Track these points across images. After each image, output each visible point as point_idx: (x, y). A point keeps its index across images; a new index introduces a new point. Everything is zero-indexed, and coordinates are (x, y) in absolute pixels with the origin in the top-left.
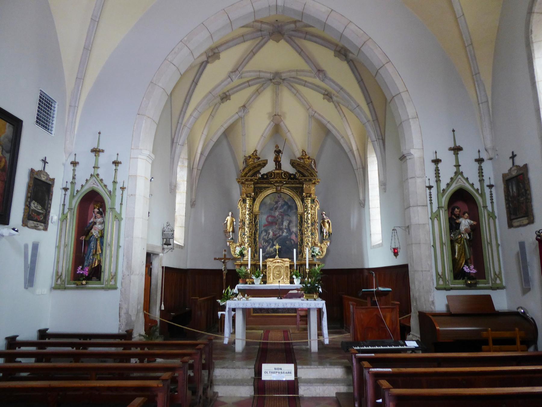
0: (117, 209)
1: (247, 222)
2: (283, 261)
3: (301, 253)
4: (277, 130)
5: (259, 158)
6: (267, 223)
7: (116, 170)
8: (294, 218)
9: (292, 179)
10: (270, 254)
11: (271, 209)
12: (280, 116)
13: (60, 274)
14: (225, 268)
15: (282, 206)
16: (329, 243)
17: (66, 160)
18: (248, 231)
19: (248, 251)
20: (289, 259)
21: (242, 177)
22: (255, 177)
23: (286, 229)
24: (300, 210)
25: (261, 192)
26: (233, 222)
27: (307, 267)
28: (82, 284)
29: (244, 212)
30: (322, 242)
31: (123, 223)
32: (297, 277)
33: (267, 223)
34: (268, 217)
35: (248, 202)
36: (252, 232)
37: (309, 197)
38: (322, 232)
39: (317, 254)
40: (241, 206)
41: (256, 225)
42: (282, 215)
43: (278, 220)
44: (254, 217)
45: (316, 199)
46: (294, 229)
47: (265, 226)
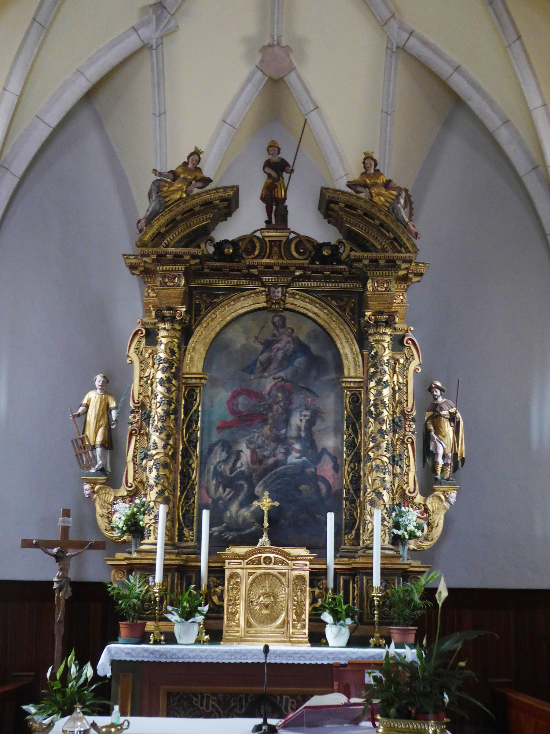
1: (157, 411)
2: (287, 556)
3: (352, 526)
4: (276, 90)
5: (208, 181)
6: (230, 418)
8: (328, 403)
9: (324, 260)
10: (239, 529)
11: (249, 369)
12: (287, 49)
14: (64, 577)
15: (288, 359)
16: (453, 495)
18: (160, 444)
19: (156, 517)
20: (310, 548)
21: (144, 245)
22: (191, 247)
23: (299, 438)
24: (352, 371)
25: (212, 306)
26: (108, 410)
27: (377, 580)
29: (149, 378)
30: (427, 491)
32: (337, 619)
33: (230, 418)
34: (234, 396)
35: (163, 337)
36: (175, 447)
37: (389, 323)
38: (427, 454)
39: (412, 535)
40: (140, 354)
41: (191, 423)
42: (287, 389)
43: (270, 408)
44: (184, 396)
45: (410, 335)
46: (329, 442)
47: (224, 426)
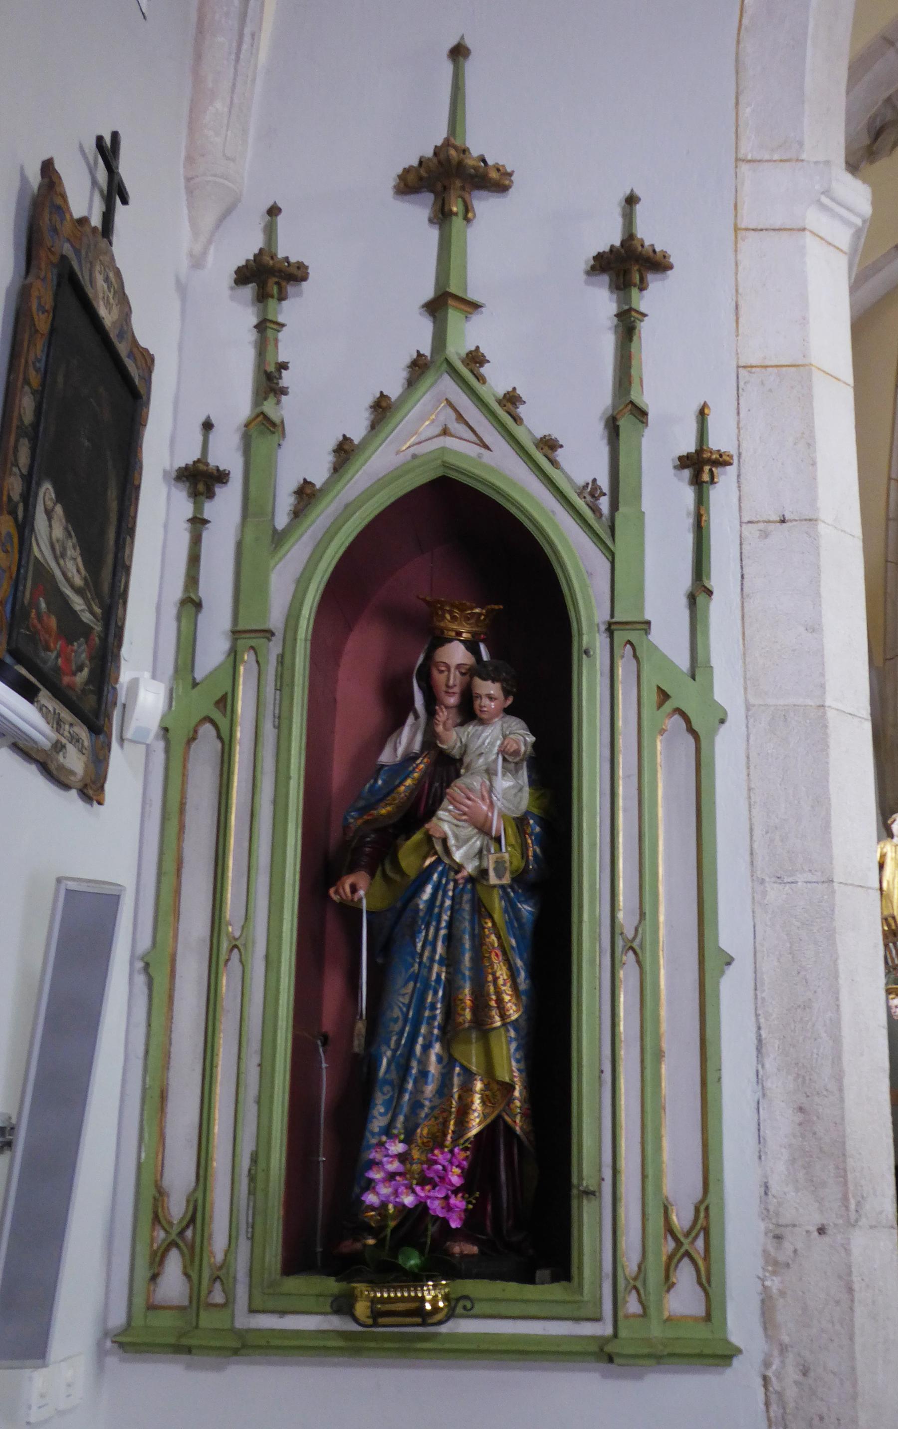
0: (669, 635)
7: (627, 325)
13: (177, 1208)
17: (197, 263)
28: (418, 1313)
31: (727, 749)
